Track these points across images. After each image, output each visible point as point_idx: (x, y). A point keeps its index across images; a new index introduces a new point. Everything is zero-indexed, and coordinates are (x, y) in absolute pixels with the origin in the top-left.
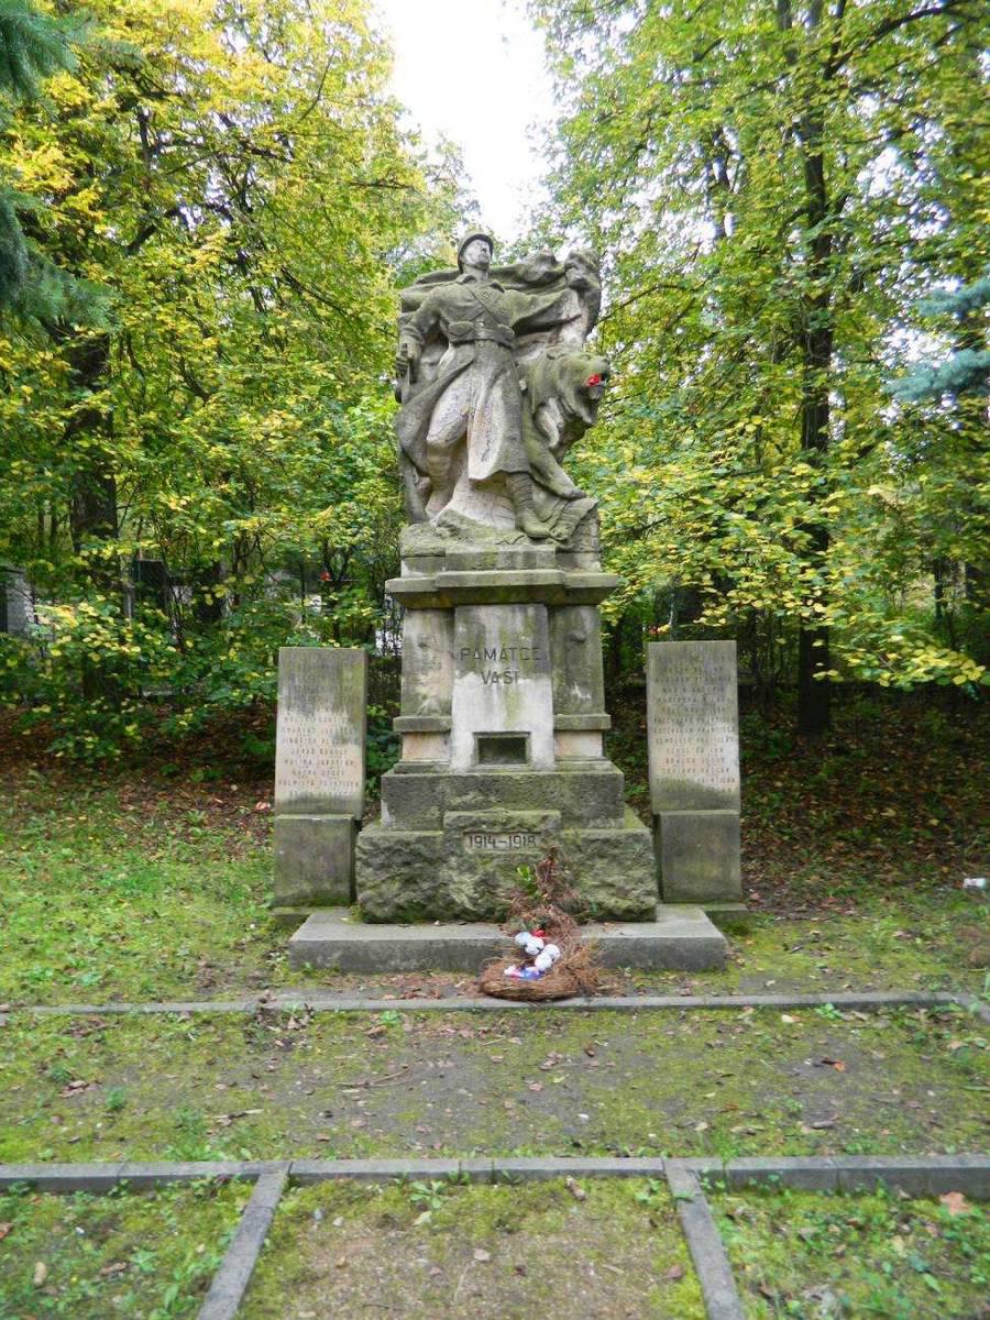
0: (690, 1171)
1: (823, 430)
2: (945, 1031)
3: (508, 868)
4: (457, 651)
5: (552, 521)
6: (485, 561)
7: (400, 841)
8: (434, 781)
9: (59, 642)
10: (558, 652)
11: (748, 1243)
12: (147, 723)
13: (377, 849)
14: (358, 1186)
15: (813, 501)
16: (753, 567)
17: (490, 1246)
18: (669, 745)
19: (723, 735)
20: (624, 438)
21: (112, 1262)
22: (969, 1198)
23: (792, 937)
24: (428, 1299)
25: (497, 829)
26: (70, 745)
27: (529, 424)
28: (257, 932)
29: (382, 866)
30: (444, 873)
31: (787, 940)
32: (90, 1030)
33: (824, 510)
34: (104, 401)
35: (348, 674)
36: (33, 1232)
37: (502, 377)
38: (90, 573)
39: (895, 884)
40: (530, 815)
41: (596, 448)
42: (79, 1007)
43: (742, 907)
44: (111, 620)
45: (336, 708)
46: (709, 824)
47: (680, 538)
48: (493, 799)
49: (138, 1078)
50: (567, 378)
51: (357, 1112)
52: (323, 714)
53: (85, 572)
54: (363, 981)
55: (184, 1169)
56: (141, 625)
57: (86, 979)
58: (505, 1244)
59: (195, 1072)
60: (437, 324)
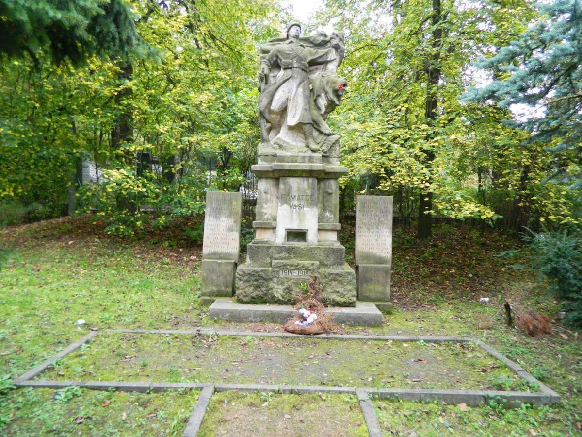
0: (365, 392)
1: (434, 111)
2: (466, 352)
3: (297, 283)
4: (280, 196)
5: (321, 144)
6: (293, 159)
7: (254, 271)
8: (269, 247)
9: (111, 185)
10: (321, 197)
11: (386, 417)
12: (145, 222)
13: (244, 274)
14: (240, 393)
15: (428, 140)
16: (402, 167)
17: (290, 413)
18: (364, 237)
19: (386, 234)
20: (350, 109)
21: (150, 414)
22: (468, 405)
23: (409, 316)
24: (268, 429)
25: (293, 268)
26: (114, 229)
27: (313, 103)
28: (194, 306)
29: (246, 281)
30: (271, 284)
31: (407, 317)
32: (130, 339)
33: (432, 144)
34: (134, 85)
35: (234, 203)
36: (119, 404)
37: (303, 84)
38: (124, 157)
39: (453, 298)
40: (307, 263)
41: (338, 113)
42: (125, 330)
43: (390, 303)
44: (133, 177)
45: (229, 216)
46: (379, 269)
47: (372, 153)
48: (292, 256)
49: (151, 356)
50: (329, 84)
51: (238, 370)
52: (223, 219)
53: (122, 156)
54: (237, 325)
55: (174, 385)
56: (145, 180)
57: (127, 320)
58: (296, 413)
59: (174, 355)
60: (277, 60)
